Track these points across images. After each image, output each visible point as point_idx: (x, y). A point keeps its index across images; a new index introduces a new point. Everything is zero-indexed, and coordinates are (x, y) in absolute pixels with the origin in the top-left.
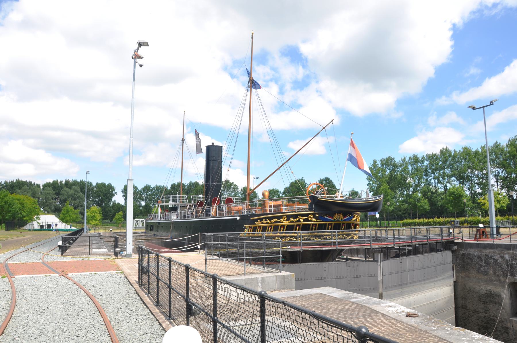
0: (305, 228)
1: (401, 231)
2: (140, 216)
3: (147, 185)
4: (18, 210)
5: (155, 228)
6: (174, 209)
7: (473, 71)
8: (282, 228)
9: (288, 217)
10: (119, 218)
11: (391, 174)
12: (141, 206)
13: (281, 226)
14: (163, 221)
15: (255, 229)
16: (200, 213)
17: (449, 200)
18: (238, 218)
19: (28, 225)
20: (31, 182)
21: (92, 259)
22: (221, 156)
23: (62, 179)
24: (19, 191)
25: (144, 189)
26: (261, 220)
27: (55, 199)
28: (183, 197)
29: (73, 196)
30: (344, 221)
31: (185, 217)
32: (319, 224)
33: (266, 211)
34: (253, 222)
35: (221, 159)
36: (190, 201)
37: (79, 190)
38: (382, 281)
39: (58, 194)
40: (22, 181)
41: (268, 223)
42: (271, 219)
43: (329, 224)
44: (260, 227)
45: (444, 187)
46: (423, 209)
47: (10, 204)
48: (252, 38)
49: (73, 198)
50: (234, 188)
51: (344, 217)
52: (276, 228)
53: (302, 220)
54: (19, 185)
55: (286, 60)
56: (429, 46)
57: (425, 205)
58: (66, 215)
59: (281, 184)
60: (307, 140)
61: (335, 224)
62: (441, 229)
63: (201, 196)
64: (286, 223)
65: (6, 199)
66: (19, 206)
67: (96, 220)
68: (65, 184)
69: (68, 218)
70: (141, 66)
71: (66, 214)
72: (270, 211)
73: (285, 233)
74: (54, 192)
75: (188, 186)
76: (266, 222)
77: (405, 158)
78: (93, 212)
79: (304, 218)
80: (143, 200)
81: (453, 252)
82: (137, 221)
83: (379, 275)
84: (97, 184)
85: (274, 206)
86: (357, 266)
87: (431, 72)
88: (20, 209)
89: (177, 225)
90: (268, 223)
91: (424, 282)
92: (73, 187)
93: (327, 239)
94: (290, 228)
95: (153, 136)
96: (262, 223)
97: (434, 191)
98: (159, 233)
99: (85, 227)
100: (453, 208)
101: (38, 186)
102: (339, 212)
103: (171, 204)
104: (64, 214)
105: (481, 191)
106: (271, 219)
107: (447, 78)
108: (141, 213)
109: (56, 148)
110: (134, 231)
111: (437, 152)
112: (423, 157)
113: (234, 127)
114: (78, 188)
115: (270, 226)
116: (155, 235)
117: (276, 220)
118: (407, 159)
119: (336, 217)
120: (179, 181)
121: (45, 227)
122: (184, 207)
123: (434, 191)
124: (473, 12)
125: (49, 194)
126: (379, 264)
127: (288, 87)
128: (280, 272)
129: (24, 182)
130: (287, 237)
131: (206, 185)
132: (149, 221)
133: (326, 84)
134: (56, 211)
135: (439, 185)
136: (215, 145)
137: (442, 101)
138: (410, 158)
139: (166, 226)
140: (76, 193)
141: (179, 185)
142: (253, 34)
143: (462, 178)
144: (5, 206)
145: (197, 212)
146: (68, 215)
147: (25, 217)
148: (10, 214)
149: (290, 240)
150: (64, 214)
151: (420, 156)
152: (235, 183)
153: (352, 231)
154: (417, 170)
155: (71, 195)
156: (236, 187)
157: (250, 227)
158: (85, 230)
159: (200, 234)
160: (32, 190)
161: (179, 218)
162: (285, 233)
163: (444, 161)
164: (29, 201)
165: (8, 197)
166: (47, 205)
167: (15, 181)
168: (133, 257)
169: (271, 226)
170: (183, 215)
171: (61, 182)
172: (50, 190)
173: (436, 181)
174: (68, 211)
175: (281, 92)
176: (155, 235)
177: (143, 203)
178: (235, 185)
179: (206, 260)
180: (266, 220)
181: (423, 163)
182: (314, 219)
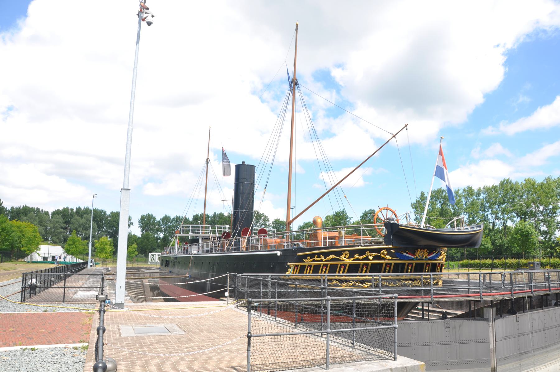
0: (376, 268)
1: (517, 275)
3: (166, 216)
4: (16, 238)
5: (171, 264)
6: (195, 241)
7: (523, 99)
8: (342, 269)
9: (352, 253)
10: (133, 251)
11: (442, 208)
12: (159, 239)
13: (341, 265)
14: (181, 255)
15: (302, 269)
16: (226, 247)
17: (516, 238)
18: (279, 253)
19: (26, 258)
20: (39, 209)
21: (61, 311)
22: (254, 178)
23: (73, 206)
24: (25, 218)
25: (163, 220)
26: (312, 256)
27: (64, 228)
28: (206, 227)
29: (84, 226)
30: (429, 259)
31: (207, 251)
32: (395, 264)
33: (318, 244)
34: (301, 259)
35: (254, 182)
36: (214, 232)
38: (495, 350)
39: (67, 223)
40: (29, 207)
41: (322, 261)
42: (326, 255)
43: (409, 264)
44: (310, 266)
45: (504, 223)
46: (484, 248)
47: (8, 232)
48: (297, 29)
49: (84, 228)
50: (264, 220)
51: (430, 253)
52: (333, 269)
53: (371, 258)
54: (25, 212)
55: (319, 85)
56: (476, 72)
57: (485, 242)
58: (72, 246)
59: (322, 212)
60: (343, 172)
61: (416, 264)
62: (530, 275)
63: (228, 226)
64: (346, 260)
66: (19, 234)
67: (106, 253)
68: (76, 212)
69: (73, 250)
70: (149, 24)
71: (72, 245)
72: (325, 243)
73: (346, 276)
74: (64, 221)
75: (211, 217)
76: (318, 259)
77: (458, 190)
78: (103, 243)
79: (374, 254)
80: (161, 232)
82: (153, 255)
83: (491, 339)
84: (112, 213)
85: (331, 238)
86: (460, 326)
87: (479, 99)
88: (19, 238)
89: (198, 261)
90: (322, 261)
91: (545, 350)
92: (85, 215)
93: (405, 285)
94: (353, 268)
95: (176, 165)
96: (314, 261)
97: (491, 228)
98: (176, 270)
99: (90, 261)
100: (520, 248)
101: (47, 213)
102: (423, 248)
103: (191, 235)
104: (69, 245)
105: (546, 229)
106: (326, 255)
107: (497, 106)
108: (158, 247)
109: (66, 172)
110: (130, 266)
111: (497, 183)
112: (479, 190)
113: (265, 155)
115: (324, 265)
116: (170, 272)
117: (334, 256)
118: (460, 192)
119: (418, 254)
120: (203, 212)
121: (50, 260)
122: (207, 239)
123: (491, 228)
124: (528, 36)
125: (58, 222)
126: (491, 323)
127: (321, 113)
128: (395, 359)
129: (32, 208)
130: (349, 281)
131: (235, 212)
132: (165, 255)
133: (364, 110)
134: (62, 241)
135: (497, 221)
136: (246, 163)
137: (489, 131)
138: (464, 190)
139: (185, 262)
141: (202, 216)
142: (297, 25)
143: (524, 215)
144: (2, 233)
145: (223, 245)
146: (74, 246)
147: (23, 246)
148: (7, 243)
149: (354, 286)
150: (69, 245)
151: (475, 188)
152: (265, 214)
153: (437, 275)
154: (473, 203)
155: (83, 224)
156: (266, 220)
157: (296, 266)
158: (90, 264)
159: (229, 274)
160: (39, 218)
161: (200, 252)
162: (346, 276)
163: (505, 194)
164: (28, 227)
165: (6, 224)
166: (56, 235)
167: (21, 208)
168: (126, 309)
169: (326, 265)
170: (205, 248)
171: (72, 210)
172: (59, 218)
173: (494, 216)
174: (74, 242)
175: (313, 119)
176: (170, 272)
177: (161, 235)
178: (266, 217)
179: (249, 337)
180: (319, 257)
181: (479, 196)
182: (388, 257)
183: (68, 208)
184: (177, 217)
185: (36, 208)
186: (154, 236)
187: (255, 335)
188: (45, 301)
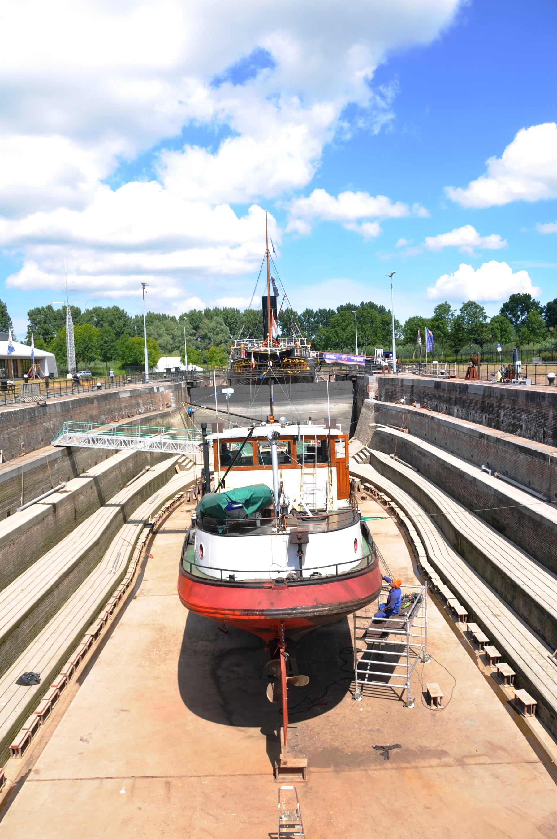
2: (345, 349)
3: (307, 309)
25: (304, 315)
37: (222, 321)
49: (215, 333)
65: (126, 344)
68: (205, 314)
81: (353, 382)
84: (246, 311)
114: (220, 319)
129: (157, 315)
140: (219, 326)
148: (131, 359)
165: (128, 342)
183: (195, 310)
184: (320, 310)
185: (161, 314)
186: (203, 331)
187: (436, 658)
188: (206, 574)
